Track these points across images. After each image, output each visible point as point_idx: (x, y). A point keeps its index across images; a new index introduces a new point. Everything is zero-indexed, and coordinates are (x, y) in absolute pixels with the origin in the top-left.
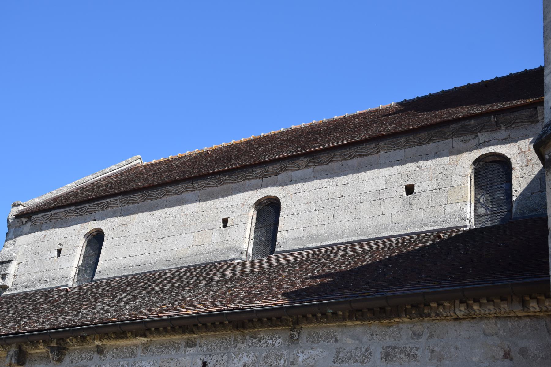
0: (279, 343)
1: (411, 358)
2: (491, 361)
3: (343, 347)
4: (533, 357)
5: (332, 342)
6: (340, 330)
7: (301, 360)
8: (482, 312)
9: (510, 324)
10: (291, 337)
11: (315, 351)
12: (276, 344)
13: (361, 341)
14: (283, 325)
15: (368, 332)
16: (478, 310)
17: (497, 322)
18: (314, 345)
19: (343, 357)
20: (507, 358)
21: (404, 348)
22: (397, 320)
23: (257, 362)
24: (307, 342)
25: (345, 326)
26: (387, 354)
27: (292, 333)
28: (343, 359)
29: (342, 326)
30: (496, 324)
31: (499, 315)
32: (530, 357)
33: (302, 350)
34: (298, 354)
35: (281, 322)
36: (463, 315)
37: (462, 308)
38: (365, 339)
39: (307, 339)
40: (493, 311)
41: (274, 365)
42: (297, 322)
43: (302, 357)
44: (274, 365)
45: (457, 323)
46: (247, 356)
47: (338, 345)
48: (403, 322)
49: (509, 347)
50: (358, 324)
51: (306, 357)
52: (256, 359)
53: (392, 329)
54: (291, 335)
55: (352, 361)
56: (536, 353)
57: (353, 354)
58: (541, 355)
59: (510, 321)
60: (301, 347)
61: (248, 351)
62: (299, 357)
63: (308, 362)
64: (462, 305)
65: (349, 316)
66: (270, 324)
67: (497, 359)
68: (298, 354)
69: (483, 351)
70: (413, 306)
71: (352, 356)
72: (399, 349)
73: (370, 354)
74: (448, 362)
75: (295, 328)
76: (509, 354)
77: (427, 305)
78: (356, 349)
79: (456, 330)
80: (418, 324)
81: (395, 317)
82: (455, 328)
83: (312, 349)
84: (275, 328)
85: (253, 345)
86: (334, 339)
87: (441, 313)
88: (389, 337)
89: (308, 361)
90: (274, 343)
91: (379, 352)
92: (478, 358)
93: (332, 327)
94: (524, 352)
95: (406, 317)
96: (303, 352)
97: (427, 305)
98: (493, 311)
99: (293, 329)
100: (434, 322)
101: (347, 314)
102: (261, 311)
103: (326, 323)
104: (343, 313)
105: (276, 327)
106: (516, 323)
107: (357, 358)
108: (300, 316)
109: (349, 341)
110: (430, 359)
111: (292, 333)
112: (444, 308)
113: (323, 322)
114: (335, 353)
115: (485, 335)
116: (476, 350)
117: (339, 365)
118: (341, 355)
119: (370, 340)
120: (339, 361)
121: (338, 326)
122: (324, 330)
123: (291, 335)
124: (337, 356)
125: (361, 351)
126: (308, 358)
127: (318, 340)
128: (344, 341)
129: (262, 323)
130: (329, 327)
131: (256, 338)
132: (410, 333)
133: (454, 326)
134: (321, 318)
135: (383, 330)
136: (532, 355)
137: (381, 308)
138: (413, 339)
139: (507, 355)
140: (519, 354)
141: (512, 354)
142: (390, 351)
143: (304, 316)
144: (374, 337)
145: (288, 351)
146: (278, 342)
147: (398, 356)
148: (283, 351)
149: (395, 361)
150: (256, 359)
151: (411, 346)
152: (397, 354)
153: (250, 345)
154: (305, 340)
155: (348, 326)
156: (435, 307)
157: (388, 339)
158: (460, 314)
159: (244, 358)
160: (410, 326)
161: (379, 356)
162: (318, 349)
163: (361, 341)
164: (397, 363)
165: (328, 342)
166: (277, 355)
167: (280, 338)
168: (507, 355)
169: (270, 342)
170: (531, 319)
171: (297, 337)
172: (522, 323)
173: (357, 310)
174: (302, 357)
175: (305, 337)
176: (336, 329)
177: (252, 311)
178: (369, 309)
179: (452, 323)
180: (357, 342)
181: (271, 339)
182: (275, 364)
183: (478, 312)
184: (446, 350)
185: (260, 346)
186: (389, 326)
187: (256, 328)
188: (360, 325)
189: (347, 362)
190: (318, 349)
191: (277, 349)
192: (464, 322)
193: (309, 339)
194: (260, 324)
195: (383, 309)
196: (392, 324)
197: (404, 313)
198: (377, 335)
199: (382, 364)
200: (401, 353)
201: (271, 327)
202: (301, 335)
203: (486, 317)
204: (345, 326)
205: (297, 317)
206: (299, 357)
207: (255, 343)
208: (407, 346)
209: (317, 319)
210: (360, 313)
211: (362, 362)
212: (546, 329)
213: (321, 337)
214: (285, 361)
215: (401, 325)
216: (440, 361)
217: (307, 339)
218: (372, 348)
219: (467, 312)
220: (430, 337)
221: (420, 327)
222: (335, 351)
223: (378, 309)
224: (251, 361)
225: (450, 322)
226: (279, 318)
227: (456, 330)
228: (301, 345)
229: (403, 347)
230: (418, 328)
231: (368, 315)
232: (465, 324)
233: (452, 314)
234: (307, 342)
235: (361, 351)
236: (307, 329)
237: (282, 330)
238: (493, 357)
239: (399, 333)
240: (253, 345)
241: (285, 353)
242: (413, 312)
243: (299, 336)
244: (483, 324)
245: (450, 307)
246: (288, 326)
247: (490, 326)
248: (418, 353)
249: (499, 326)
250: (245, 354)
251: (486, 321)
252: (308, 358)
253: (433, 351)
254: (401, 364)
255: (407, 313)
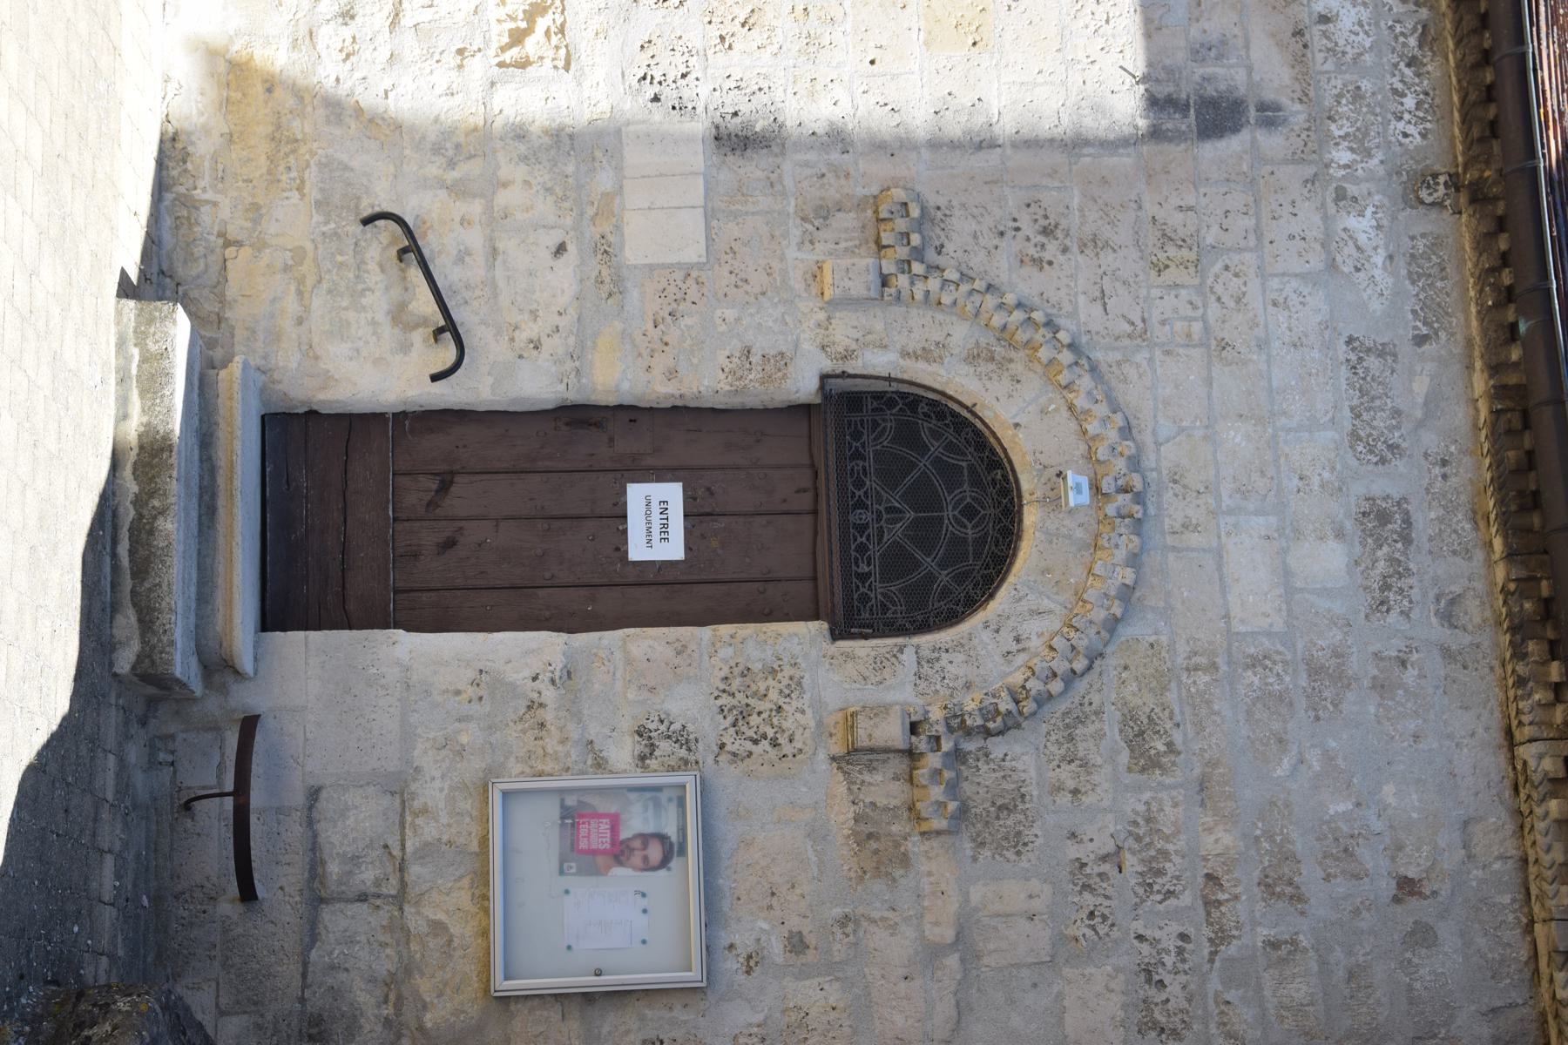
0: (1406, 135)
1: (1377, 594)
2: (1387, 840)
3: (1398, 367)
4: (1409, 961)
5: (1415, 328)
6: (1457, 350)
7: (1352, 222)
8: (1541, 826)
9: (1507, 899)
10: (1427, 178)
11: (1385, 268)
12: (1401, 125)
13: (1420, 424)
14: (1468, 147)
15: (1453, 448)
16: (1547, 814)
17: (1510, 862)
18: (1402, 263)
19: (1367, 369)
20: (1400, 886)
21: (1407, 569)
22: (1498, 544)
23: (1339, 65)
24: (1413, 238)
25: (1470, 367)
26: (1384, 518)
27: (1442, 179)
28: (1360, 371)
29: (1470, 356)
30: (1502, 857)
31: (1532, 869)
32: (1408, 955)
33: (1385, 223)
34: (1370, 210)
35: (1481, 140)
36: (1525, 763)
37: (1548, 765)
38: (1430, 440)
39: (1423, 235)
40: (1546, 859)
41: (1333, 127)
42: (1478, 196)
43: (1361, 225)
44: (1333, 127)
45: (1498, 736)
46: (1360, 24)
47: (1406, 348)
48: (1490, 564)
49: (1435, 893)
50: (1477, 410)
51: (1362, 239)
52: (1349, 57)
53: (1468, 526)
54: (1435, 176)
55: (1355, 402)
56: (1421, 971)
57: (1377, 403)
58: (1417, 985)
59: (1514, 900)
60: (1394, 218)
61: (1377, 24)
62: (1361, 214)
63: (1346, 251)
64: (1560, 764)
65: (1504, 387)
66: (1473, 97)
67: (1393, 859)
68: (1370, 210)
69: (1415, 815)
70: (1547, 603)
71: (1373, 399)
72: (1404, 553)
73: (1383, 461)
74: (1372, 709)
75: (1457, 190)
76: (1411, 893)
77: (1553, 651)
78: (1397, 413)
79: (1473, 735)
80: (1488, 614)
81: (1506, 544)
82: (1481, 730)
83: (1391, 257)
84: (1456, 114)
85: (1396, 38)
86: (1425, 331)
87: (1530, 695)
88: (1441, 520)
89: (1350, 249)
90: (1407, 116)
91: (1389, 491)
92: (1391, 800)
93: (1465, 321)
94: (1422, 936)
95: (1508, 579)
96: (1379, 227)
97: (1553, 651)
98: (1546, 859)
99: (1454, 183)
100: (1496, 664)
101: (1513, 379)
102: (1521, 69)
103: (1480, 303)
104: (1516, 365)
105: (1463, 121)
106: (1511, 918)
107: (1366, 416)
108: (1500, 208)
109: (1421, 386)
110: (1377, 655)
111: (1442, 179)
112: (1549, 706)
113: (1481, 291)
114: (1379, 341)
115: (1466, 823)
116: (1415, 797)
117: (1342, 358)
118: (1373, 363)
119: (1426, 455)
120: (1353, 357)
121: (1469, 342)
122: (1455, 295)
123: (1435, 176)
124: (1369, 350)
125: (1392, 429)
126: (1358, 248)
127: (1420, 276)
128: (1418, 368)
129: (1476, 66)
130: (1466, 311)
131: (1420, 47)
132: (1456, 589)
133: (1487, 729)
134: (1496, 287)
135: (1463, 498)
136: (1416, 960)
137: (1536, 494)
138: (1438, 600)
139: (1407, 887)
140: (1416, 922)
141: (1414, 902)
142: (1396, 525)
143: (1501, 224)
144: (1437, 470)
145: (1381, 171)
146: (1411, 129)
147: (1379, 553)
148: (1379, 156)
149: (1363, 544)
150: (1349, 57)
151: (1416, 594)
152: (1385, 549)
153: (1398, 29)
154: (1417, 230)
155: (1470, 377)
156: (1548, 674)
157: (1433, 515)
158: (1527, 752)
159: (1353, 11)
160: (1479, 585)
161: (1377, 489)
162: (1390, 281)
163: (1420, 424)
164: (1358, 549)
165: (1414, 312)
166: (1366, 135)
167: (1423, 136)
168: (1407, 887)
169: (1410, 102)
170: (1526, 963)
171: (1429, 200)
172: (1513, 935)
173: (1525, 414)
174: (1361, 225)
175: (1428, 228)
176: (1459, 337)
177: (1520, 39)
178: (1530, 454)
179: (1496, 721)
180: (1419, 414)
181: (1419, 105)
182: (1337, 133)
183: (1539, 811)
184: (1409, 705)
185: (1396, 65)
186: (1475, 516)
187: (1458, 44)
188: (1476, 418)
189: (1351, 385)
190: (1390, 281)
191: (1386, 130)
192: (1502, 758)
193: (1421, 245)
194: (1470, 60)
195: (1532, 501)
196: (1482, 524)
197: (1523, 574)
198: (1444, 477)
199: (1353, 500)
200: (1391, 560)
201: (1463, 100)
202: (1433, 214)
203: (1522, 827)
204: (1470, 367)
205: (1496, 199)
206: (1361, 214)
207: (1404, 45)
208: (1411, 581)
209: (1492, 270)
210: (1517, 424)
211: (1355, 436)
212: (1499, 1003)
213: (1432, 285)
214: (1347, 166)
215: (1479, 555)
216: (1374, 687)
217: (1423, 235)
218: (1400, 465)
219: (1536, 778)
220: (1447, 654)
221: (1477, 620)
222: (1386, 340)
223: (1533, 487)
224: (1341, 42)
225: (1497, 714)
226: (1494, 129)
227: (1473, 735)
228: (1402, 216)
229: (1411, 566)
230: (1474, 611)
231: (1511, 454)
232: (1495, 763)
233: (1528, 731)
234: (1413, 238)
235: (1392, 429)
236: (1455, 231)
237: (1453, 137)
238: (1400, 848)
239: (1454, 552)
240: (1396, 38)
241: (1376, 161)
242: (1528, 605)
243: (1433, 204)
244: (1498, 819)
245: (1550, 725)
246: (1466, 167)
247: (1495, 836)
248: (1393, 617)
249: (1497, 866)
250: (1365, 15)
251: (1510, 827)
252: (1358, 248)
253: (1403, 663)
254: (1357, 563)
255: (1526, 585)
